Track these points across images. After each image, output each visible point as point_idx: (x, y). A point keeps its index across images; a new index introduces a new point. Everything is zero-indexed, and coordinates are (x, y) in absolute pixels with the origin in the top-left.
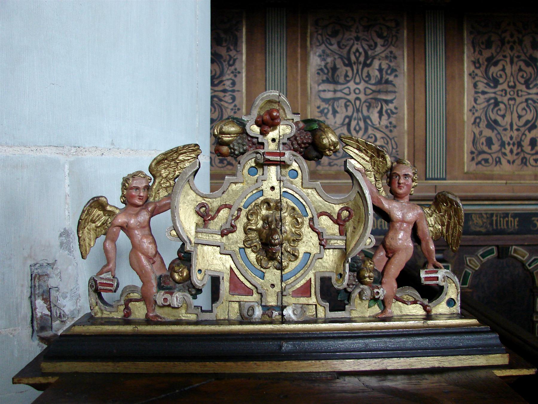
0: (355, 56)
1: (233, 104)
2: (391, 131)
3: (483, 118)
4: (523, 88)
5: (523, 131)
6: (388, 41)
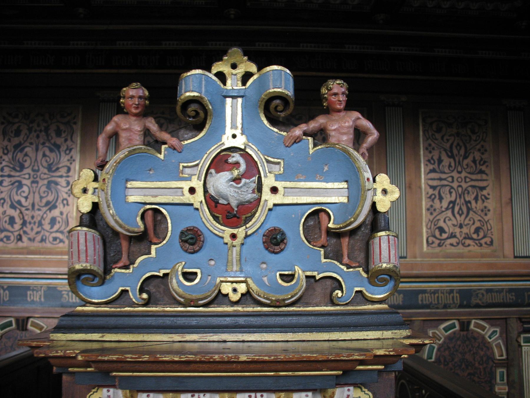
3: (8, 200)
4: (46, 171)
5: (44, 211)
6: (479, 136)
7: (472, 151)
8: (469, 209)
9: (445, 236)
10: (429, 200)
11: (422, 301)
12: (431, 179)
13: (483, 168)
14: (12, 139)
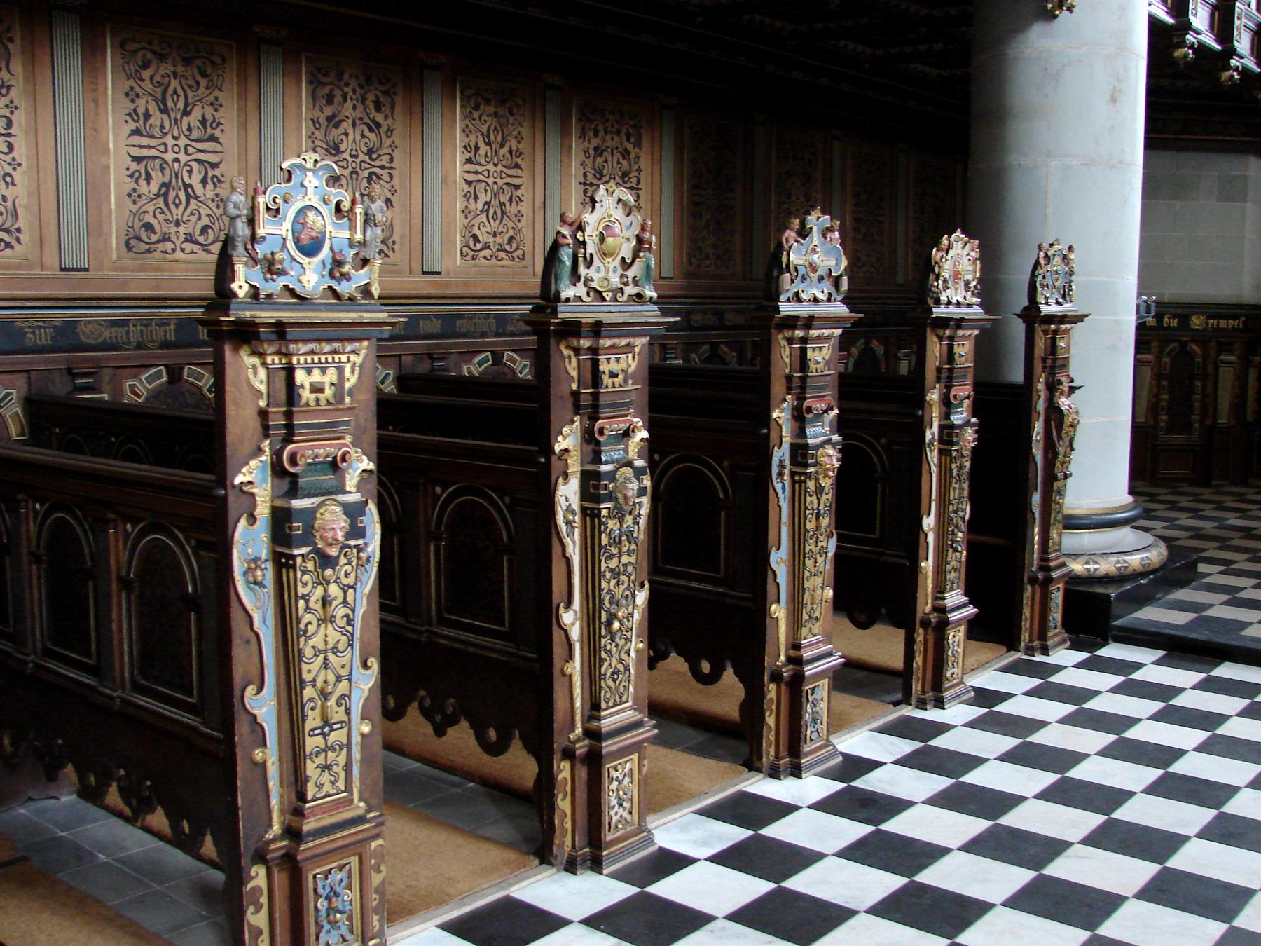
0: (179, 199)
1: (11, 156)
2: (132, 88)
7: (509, 138)
8: (503, 213)
9: (479, 246)
10: (464, 199)
11: (460, 328)
12: (468, 172)
13: (519, 161)
14: (592, 140)
